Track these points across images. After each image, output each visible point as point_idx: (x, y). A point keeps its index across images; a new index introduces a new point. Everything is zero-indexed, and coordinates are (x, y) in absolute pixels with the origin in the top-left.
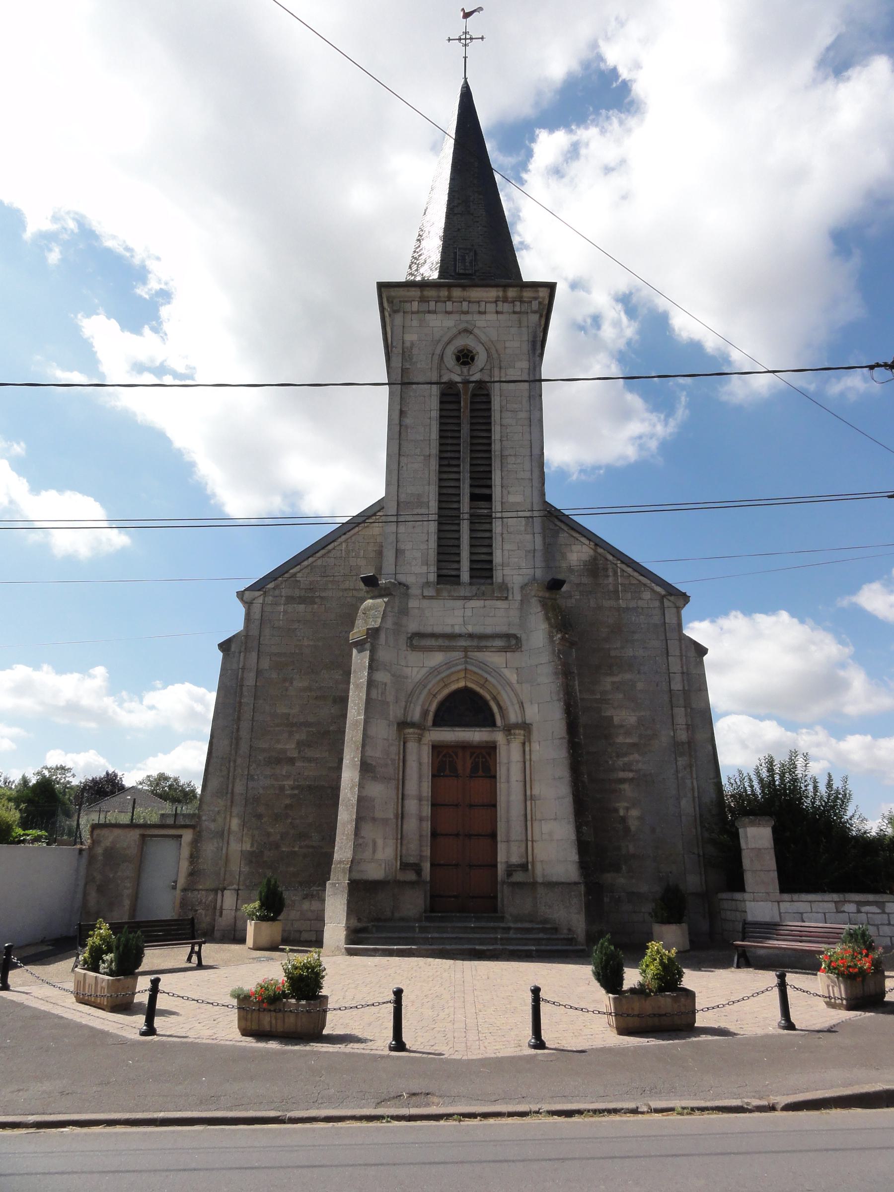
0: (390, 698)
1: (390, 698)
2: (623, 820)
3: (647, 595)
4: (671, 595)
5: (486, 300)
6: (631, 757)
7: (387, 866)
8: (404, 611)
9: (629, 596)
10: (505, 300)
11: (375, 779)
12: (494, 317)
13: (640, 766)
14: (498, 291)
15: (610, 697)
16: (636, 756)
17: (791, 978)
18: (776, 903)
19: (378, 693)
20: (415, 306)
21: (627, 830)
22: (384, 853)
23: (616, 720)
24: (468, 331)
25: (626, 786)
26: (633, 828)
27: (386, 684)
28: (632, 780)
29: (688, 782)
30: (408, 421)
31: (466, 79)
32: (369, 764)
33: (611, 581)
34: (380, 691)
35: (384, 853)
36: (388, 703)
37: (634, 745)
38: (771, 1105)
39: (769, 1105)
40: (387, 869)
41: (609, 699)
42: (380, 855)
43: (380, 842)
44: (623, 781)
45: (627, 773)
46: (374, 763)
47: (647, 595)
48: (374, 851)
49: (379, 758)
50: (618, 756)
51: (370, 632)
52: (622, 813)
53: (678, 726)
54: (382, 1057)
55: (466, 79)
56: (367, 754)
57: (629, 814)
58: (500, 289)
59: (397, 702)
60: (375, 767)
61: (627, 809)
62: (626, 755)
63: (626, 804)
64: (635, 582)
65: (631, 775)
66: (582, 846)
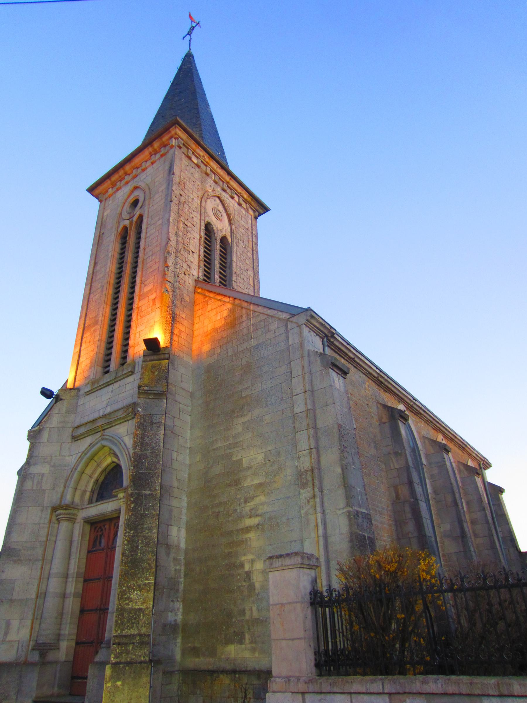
2: (248, 575)
3: (274, 326)
4: (293, 315)
5: (145, 160)
6: (257, 501)
7: (20, 647)
9: (259, 332)
10: (156, 152)
13: (266, 508)
14: (148, 149)
15: (241, 439)
16: (263, 498)
18: (300, 696)
19: (33, 484)
20: (110, 191)
21: (251, 587)
23: (246, 462)
24: (136, 188)
25: (251, 535)
26: (257, 585)
28: (257, 526)
29: (312, 518)
30: (98, 268)
32: (14, 549)
33: (245, 326)
34: (35, 482)
35: (18, 633)
37: (260, 485)
40: (20, 650)
41: (240, 442)
42: (13, 636)
43: (15, 623)
44: (248, 529)
45: (253, 519)
47: (274, 326)
50: (246, 502)
51: (32, 434)
52: (247, 568)
53: (301, 453)
55: (190, 49)
57: (254, 568)
58: (149, 147)
59: (54, 489)
60: (20, 550)
61: (252, 561)
62: (252, 498)
63: (250, 557)
64: (263, 317)
65: (256, 521)
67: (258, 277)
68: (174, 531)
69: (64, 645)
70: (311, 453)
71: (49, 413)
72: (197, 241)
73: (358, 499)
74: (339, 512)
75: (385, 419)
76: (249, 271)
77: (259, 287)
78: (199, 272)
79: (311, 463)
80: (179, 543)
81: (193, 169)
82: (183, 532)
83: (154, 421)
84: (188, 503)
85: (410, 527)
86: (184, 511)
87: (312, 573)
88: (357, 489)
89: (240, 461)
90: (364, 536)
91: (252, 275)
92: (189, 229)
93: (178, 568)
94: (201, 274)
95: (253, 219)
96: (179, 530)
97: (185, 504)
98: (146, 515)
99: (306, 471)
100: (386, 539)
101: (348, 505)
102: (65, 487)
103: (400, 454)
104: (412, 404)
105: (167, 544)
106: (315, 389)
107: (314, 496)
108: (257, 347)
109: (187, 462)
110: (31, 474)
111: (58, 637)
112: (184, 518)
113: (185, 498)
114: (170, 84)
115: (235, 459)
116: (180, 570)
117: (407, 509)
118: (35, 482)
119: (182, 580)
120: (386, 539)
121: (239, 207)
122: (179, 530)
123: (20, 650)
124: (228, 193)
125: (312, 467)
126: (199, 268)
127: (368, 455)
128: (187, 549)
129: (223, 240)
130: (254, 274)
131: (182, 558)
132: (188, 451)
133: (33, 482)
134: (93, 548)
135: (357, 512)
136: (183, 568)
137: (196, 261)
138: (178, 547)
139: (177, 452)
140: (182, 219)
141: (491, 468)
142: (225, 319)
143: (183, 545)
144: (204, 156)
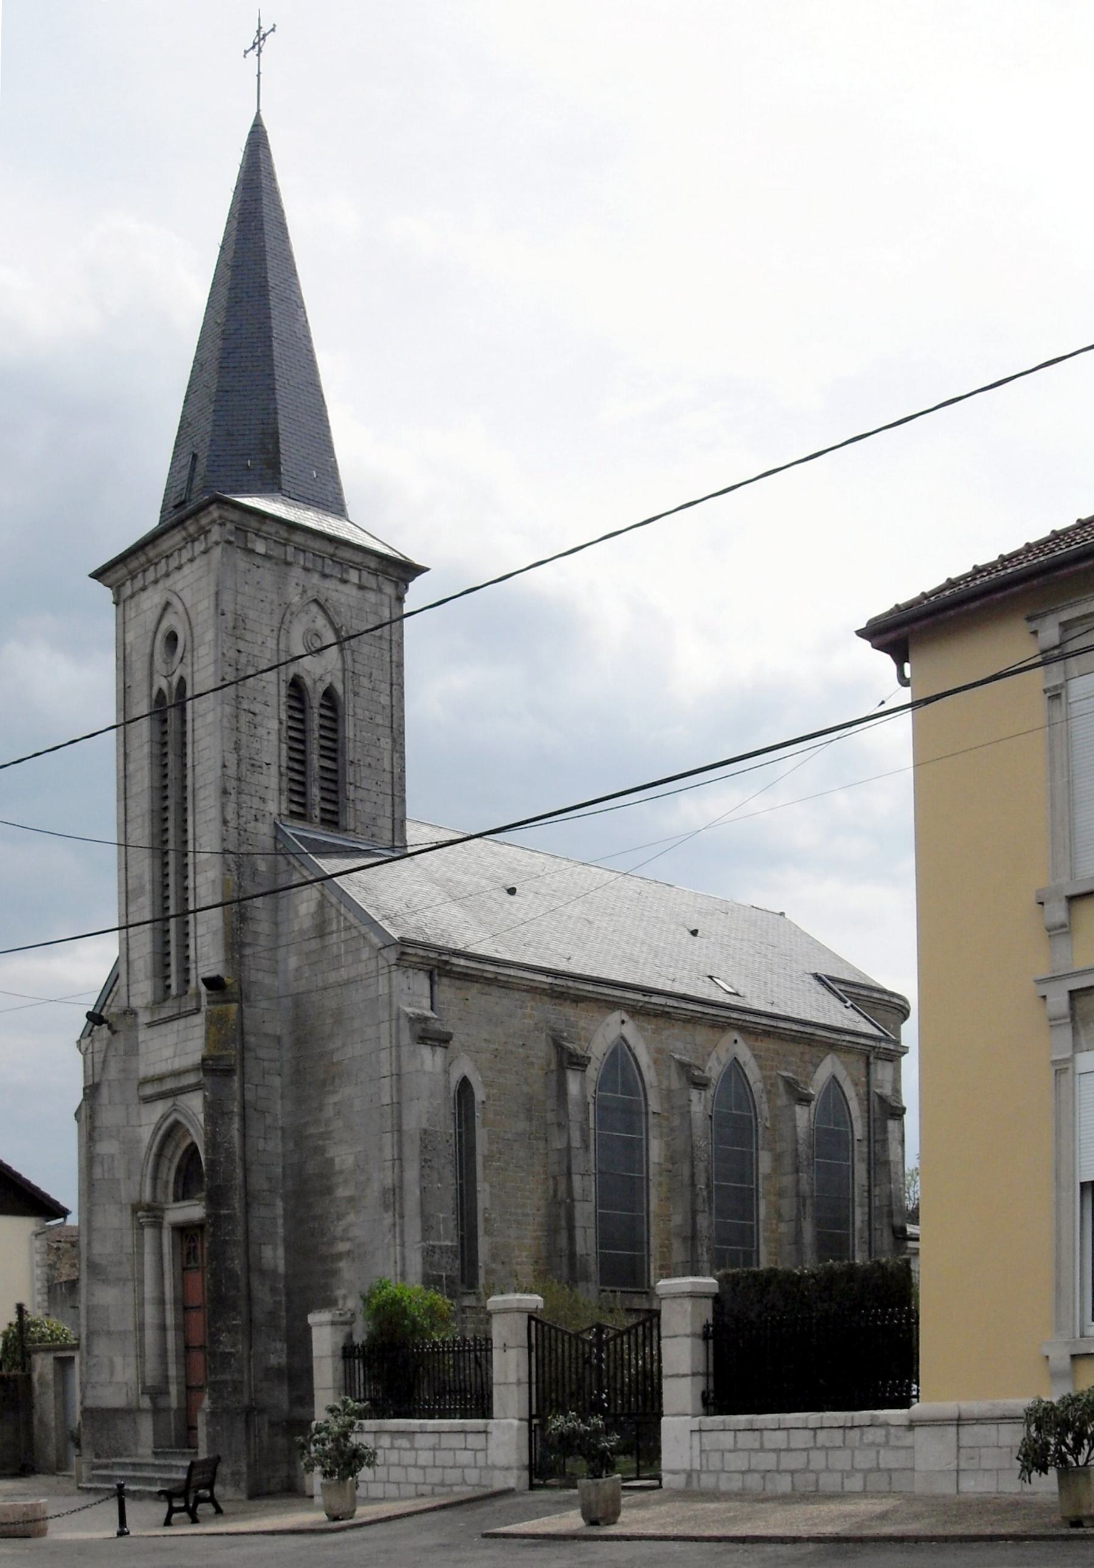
0: (120, 1174)
1: (120, 1174)
8: (133, 1051)
11: (106, 1281)
12: (354, 591)
17: (840, 1490)
19: (103, 1170)
22: (124, 1373)
27: (112, 1156)
31: (259, 111)
36: (119, 1180)
38: (546, 1234)
39: (547, 1236)
42: (119, 1377)
43: (118, 1361)
46: (104, 1262)
48: (112, 1374)
49: (110, 1255)
54: (1074, 1176)
55: (259, 111)
56: (95, 1251)
66: (715, 1311)
67: (402, 745)
68: (267, 1252)
69: (173, 1389)
70: (393, 1165)
71: (115, 989)
72: (274, 737)
73: (439, 1230)
74: (416, 1246)
75: (553, 1066)
76: (382, 739)
77: (403, 771)
78: (280, 803)
79: (393, 1180)
80: (276, 1266)
81: (261, 570)
82: (281, 1252)
83: (225, 1110)
84: (285, 1210)
85: (563, 1240)
86: (280, 1221)
87: (347, 1329)
88: (438, 1217)
89: (332, 1159)
90: (441, 1276)
91: (389, 747)
92: (258, 718)
93: (278, 1299)
94: (284, 805)
95: (393, 602)
96: (275, 1249)
97: (280, 1211)
98: (227, 1241)
99: (389, 1189)
100: (524, 1259)
101: (424, 1239)
102: (142, 1176)
103: (564, 1126)
104: (641, 1004)
105: (260, 1270)
106: (403, 1071)
107: (394, 1225)
108: (347, 983)
109: (280, 1150)
110: (99, 1155)
111: (166, 1378)
112: (281, 1231)
113: (280, 1204)
114: (219, 249)
115: (327, 1156)
116: (280, 1303)
117: (563, 1212)
118: (106, 1167)
119: (283, 1314)
120: (524, 1259)
121: (361, 593)
122: (275, 1249)
123: (130, 1394)
124: (336, 577)
125: (394, 1185)
126: (280, 794)
127: (509, 1136)
128: (286, 1276)
129: (329, 694)
130: (394, 740)
131: (281, 1286)
132: (279, 1133)
133: (103, 1166)
134: (188, 1263)
135: (433, 1247)
136: (283, 1298)
137: (274, 782)
138: (274, 1271)
139: (265, 1138)
140: (245, 705)
141: (910, 1049)
142: (313, 918)
143: (281, 1269)
144: (277, 532)
